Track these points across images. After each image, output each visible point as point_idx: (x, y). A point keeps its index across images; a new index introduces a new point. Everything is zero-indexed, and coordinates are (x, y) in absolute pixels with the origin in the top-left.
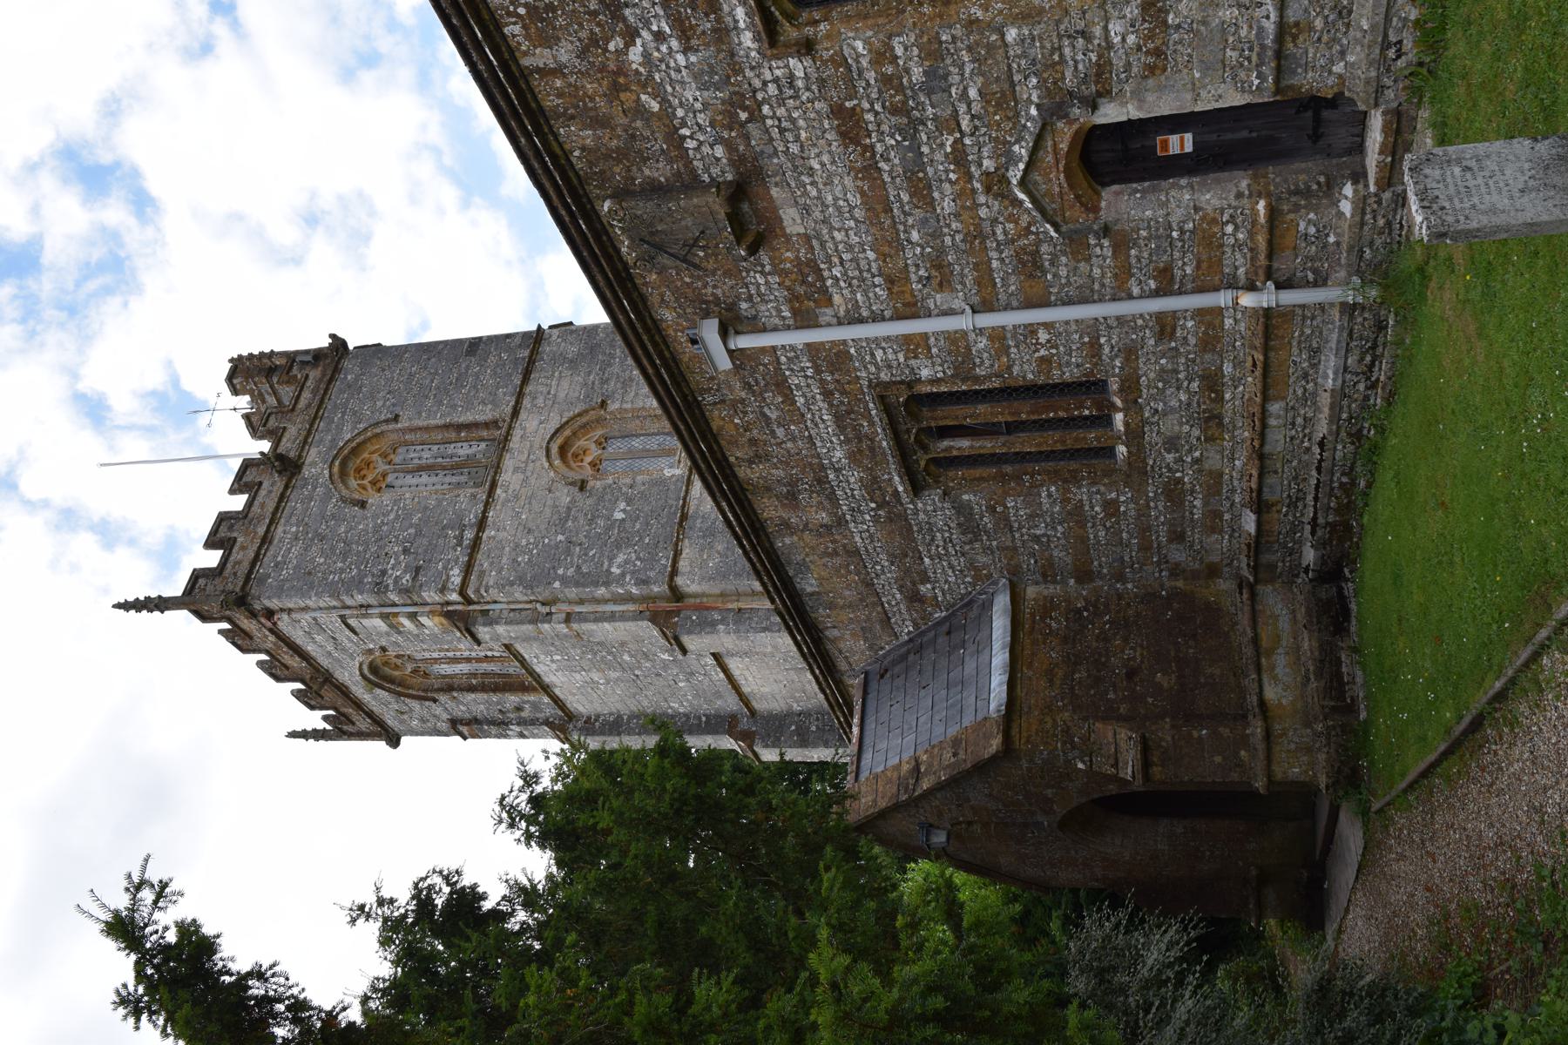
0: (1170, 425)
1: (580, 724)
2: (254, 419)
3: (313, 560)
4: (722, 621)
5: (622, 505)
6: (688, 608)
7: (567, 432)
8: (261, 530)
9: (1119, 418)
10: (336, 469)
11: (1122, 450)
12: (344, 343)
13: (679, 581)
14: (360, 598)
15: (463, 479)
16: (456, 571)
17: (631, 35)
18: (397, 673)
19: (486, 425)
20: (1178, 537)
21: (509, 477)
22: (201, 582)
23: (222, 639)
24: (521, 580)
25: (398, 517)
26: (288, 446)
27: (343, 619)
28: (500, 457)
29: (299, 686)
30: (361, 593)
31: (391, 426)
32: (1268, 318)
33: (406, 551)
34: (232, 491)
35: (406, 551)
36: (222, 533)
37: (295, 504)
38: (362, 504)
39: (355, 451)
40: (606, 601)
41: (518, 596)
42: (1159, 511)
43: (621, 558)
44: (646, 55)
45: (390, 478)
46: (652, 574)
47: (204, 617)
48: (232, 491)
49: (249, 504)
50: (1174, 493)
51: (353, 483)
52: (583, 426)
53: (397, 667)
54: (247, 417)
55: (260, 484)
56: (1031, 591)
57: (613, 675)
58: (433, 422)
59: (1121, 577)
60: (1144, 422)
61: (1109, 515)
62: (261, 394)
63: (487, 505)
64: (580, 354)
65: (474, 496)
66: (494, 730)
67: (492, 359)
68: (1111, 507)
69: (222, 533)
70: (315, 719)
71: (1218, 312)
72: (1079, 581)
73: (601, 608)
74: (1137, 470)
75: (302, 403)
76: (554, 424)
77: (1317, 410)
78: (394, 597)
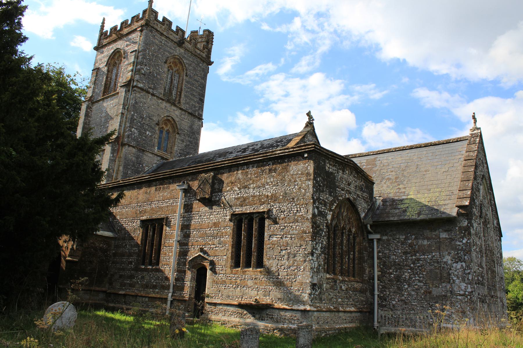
0: (147, 277)
1: (90, 105)
2: (196, 34)
3: (153, 46)
4: (113, 156)
5: (150, 134)
6: (119, 147)
7: (173, 122)
8: (165, 33)
9: (151, 267)
10: (177, 57)
11: (143, 267)
12: (210, 65)
13: (127, 147)
14: (140, 57)
15: (166, 91)
16: (142, 86)
17: (240, 189)
18: (116, 57)
19: (179, 100)
20: (121, 276)
21: (164, 104)
22: (154, 14)
23: (137, 14)
24: (136, 103)
25: (160, 72)
26: (187, 44)
27: (136, 51)
28: (170, 103)
29: (119, 28)
30: (142, 58)
31: (185, 74)
32: (166, 299)
33: (150, 72)
34: (177, 27)
35: (150, 72)
36: (167, 22)
37: (170, 44)
38: (166, 63)
39: (180, 63)
40: (125, 125)
41: (131, 101)
42: (128, 273)
43: (136, 131)
44: (236, 191)
45: (171, 71)
46: (130, 139)
47: (144, 12)
48: (177, 27)
49: (172, 31)
50: (131, 277)
51: (172, 60)
52: (173, 127)
53: (118, 58)
54: (197, 32)
55: (177, 35)
56: (113, 242)
57: (103, 119)
58: (184, 85)
59: (113, 263)
60: (149, 273)
61: (129, 262)
62: (202, 38)
63: (158, 97)
64: (193, 129)
65: (161, 94)
66: (93, 79)
67: (197, 105)
68: (131, 263)
69: (166, 22)
70: (107, 28)
71: (169, 289)
72: (114, 253)
73: (124, 123)
74: (137, 269)
75: (197, 50)
76: (177, 119)
77: (145, 308)
78: (139, 67)
